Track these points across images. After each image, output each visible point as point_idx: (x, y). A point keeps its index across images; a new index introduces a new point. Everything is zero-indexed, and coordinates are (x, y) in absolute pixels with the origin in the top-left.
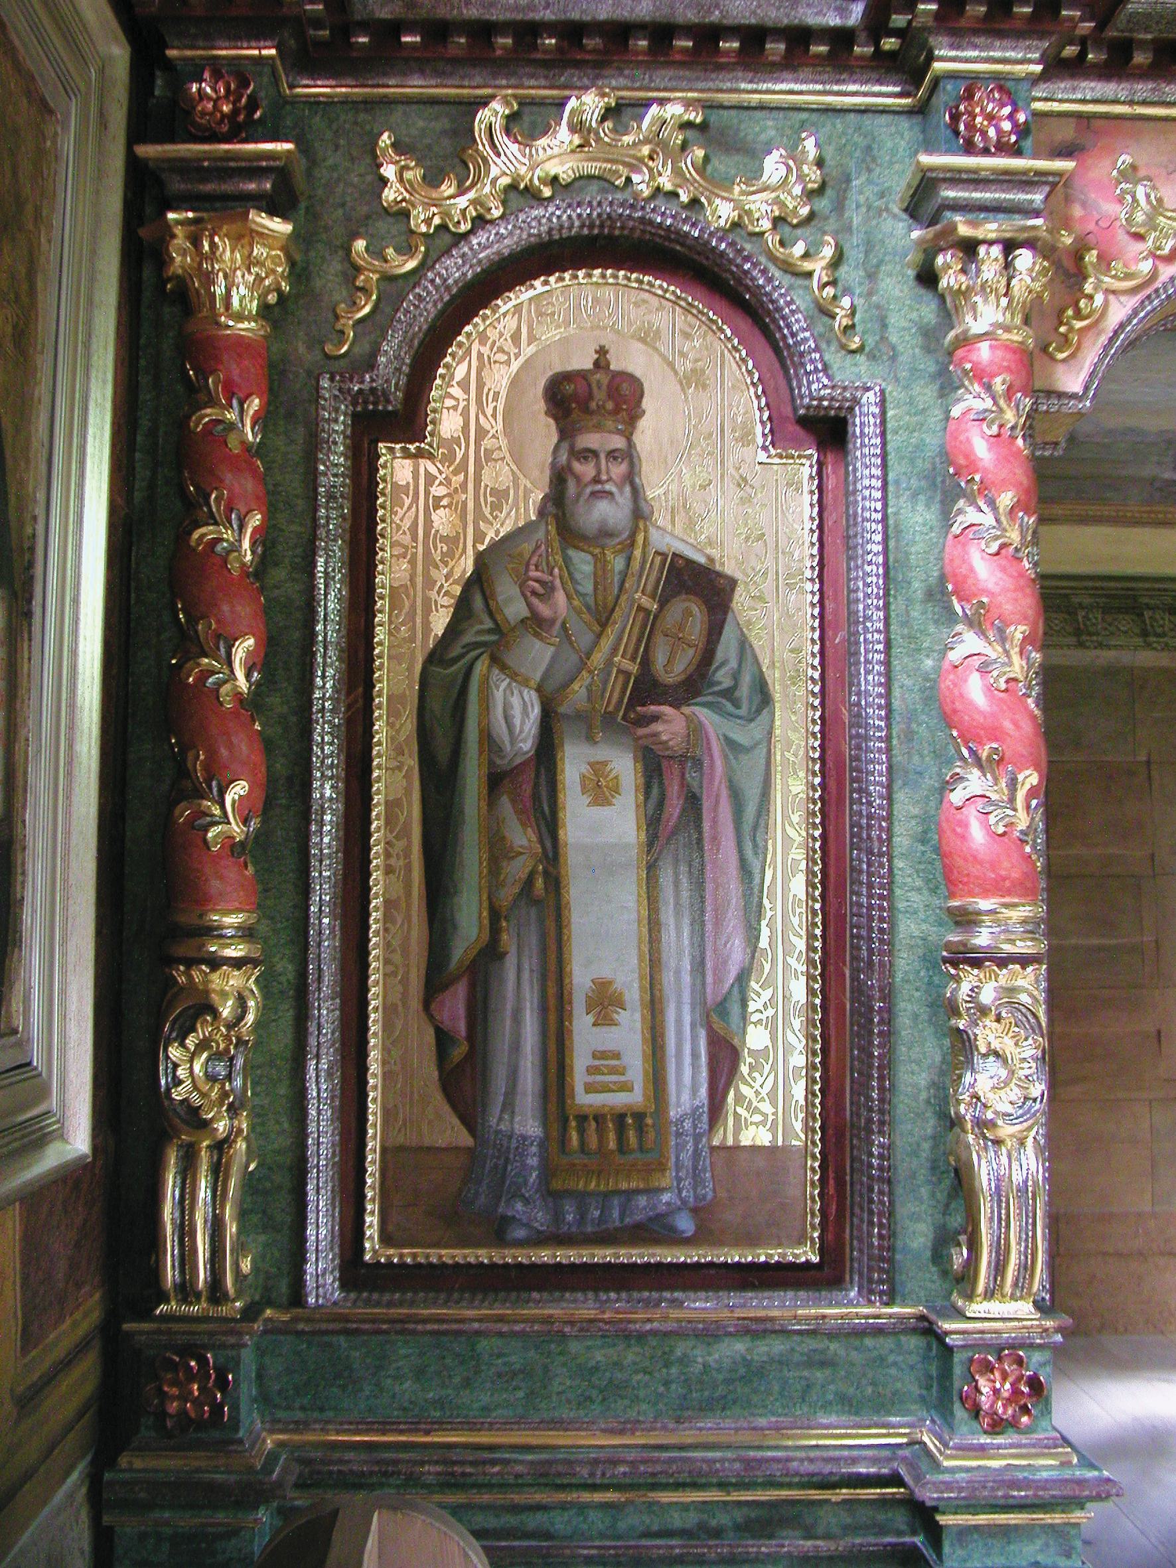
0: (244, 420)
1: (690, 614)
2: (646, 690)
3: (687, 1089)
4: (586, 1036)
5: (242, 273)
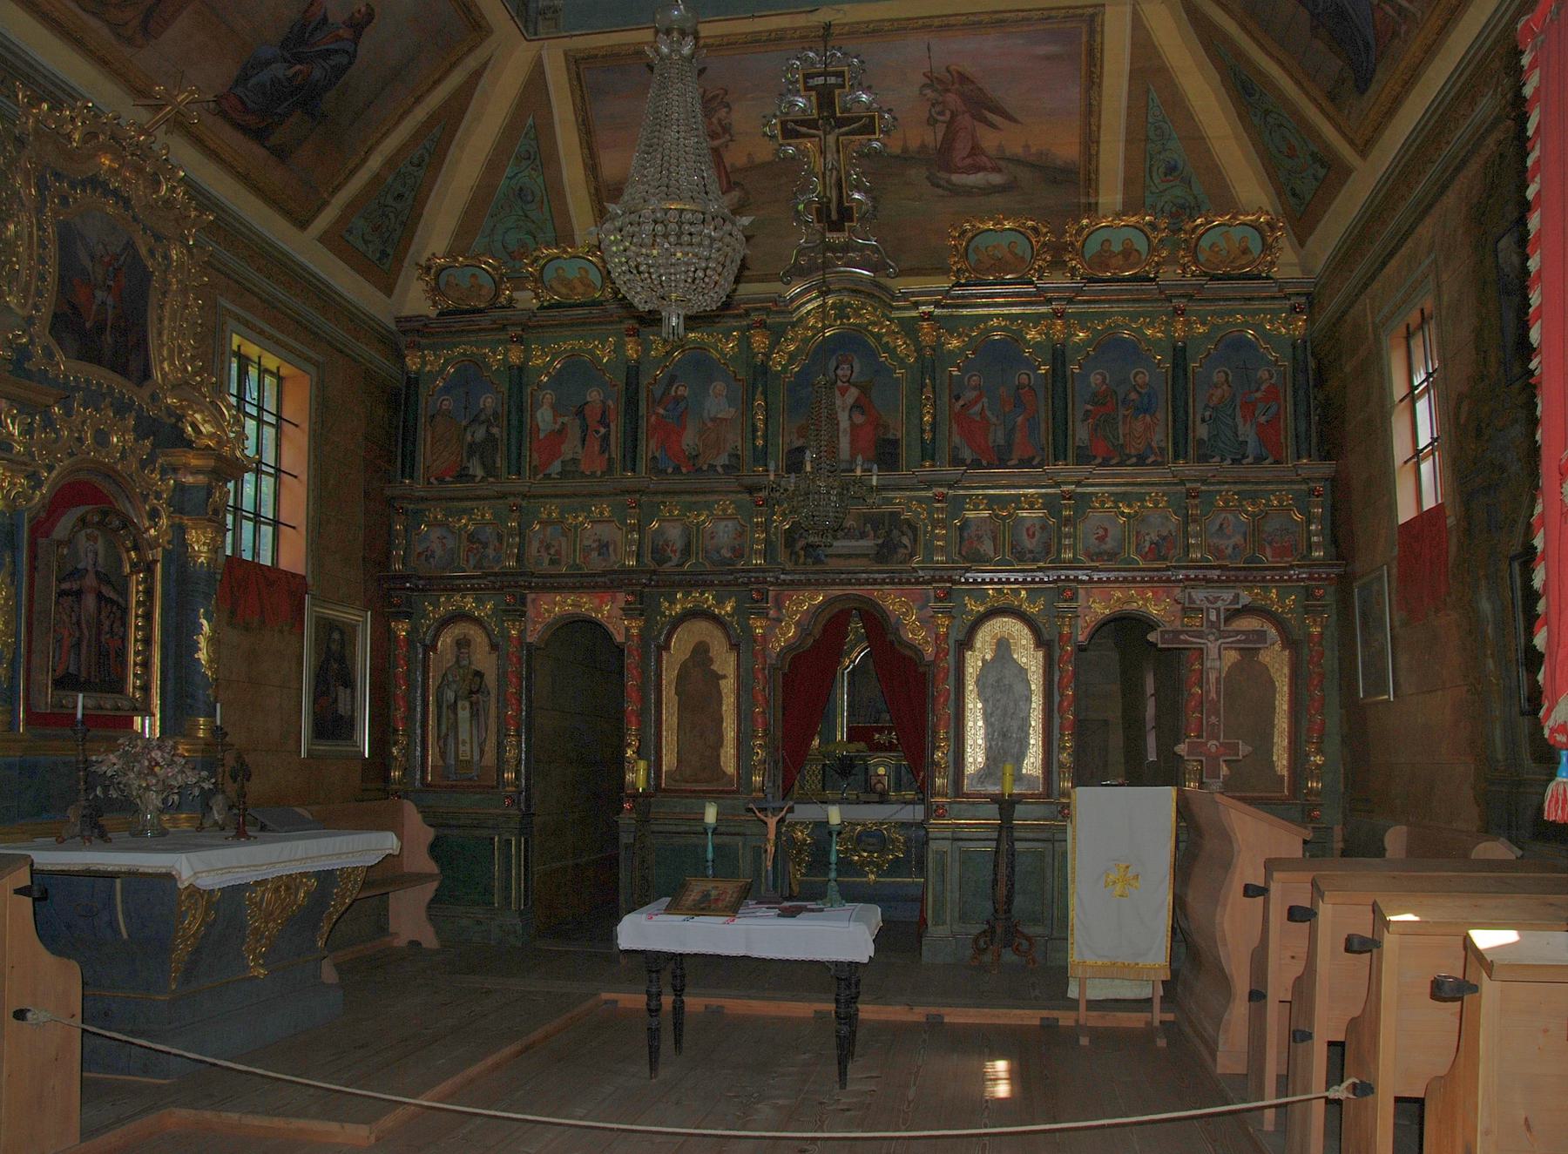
0: (402, 651)
1: (478, 679)
2: (471, 692)
3: (476, 757)
4: (461, 748)
5: (402, 629)
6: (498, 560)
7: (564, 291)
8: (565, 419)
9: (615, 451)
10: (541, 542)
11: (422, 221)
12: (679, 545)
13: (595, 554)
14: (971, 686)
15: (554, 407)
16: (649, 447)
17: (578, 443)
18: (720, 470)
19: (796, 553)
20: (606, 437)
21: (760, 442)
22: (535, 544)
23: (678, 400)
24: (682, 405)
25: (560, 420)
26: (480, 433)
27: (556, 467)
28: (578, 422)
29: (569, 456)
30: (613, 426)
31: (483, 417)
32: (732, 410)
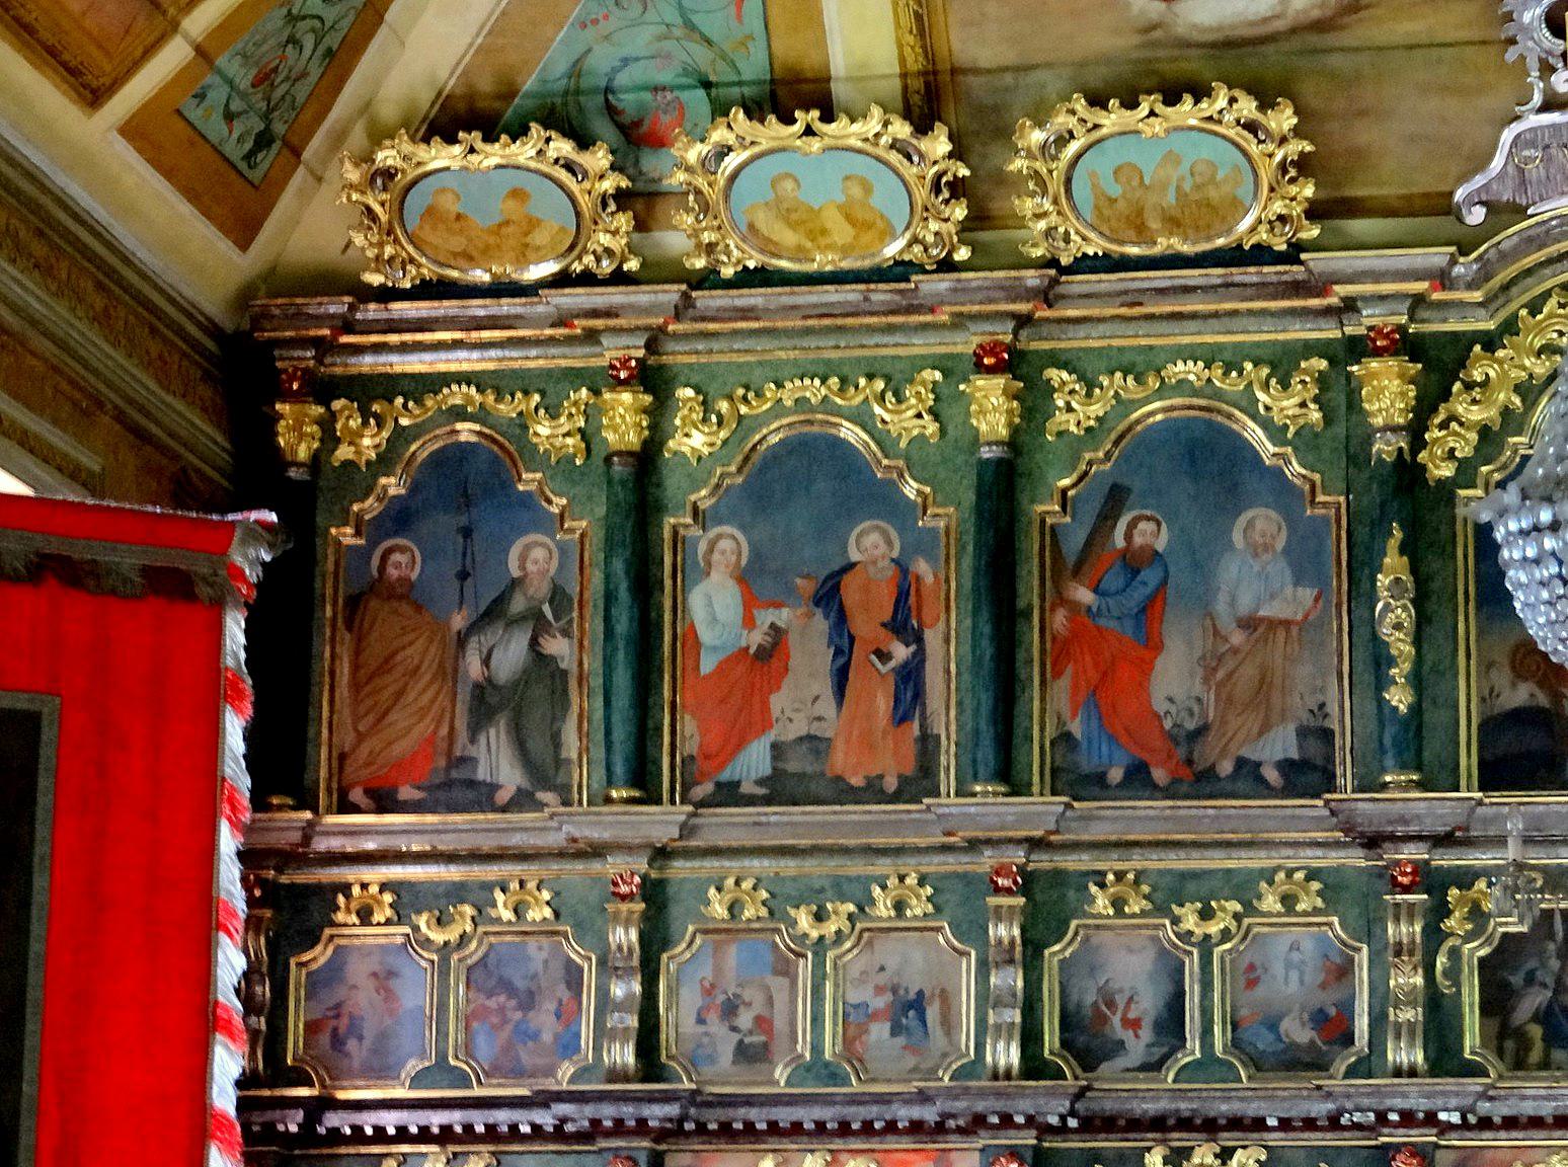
6: (568, 1046)
7: (788, 238)
8: (783, 616)
9: (948, 709)
10: (709, 991)
11: (383, 32)
12: (1149, 1004)
13: (880, 1031)
14: (1013, 273)
15: (744, 578)
16: (1052, 707)
17: (824, 686)
18: (1272, 775)
19: (1520, 1035)
20: (910, 678)
21: (1399, 698)
22: (691, 998)
23: (1134, 562)
24: (1150, 577)
25: (766, 617)
26: (510, 654)
27: (753, 762)
28: (821, 624)
29: (798, 728)
30: (932, 638)
31: (518, 605)
32: (1307, 594)
